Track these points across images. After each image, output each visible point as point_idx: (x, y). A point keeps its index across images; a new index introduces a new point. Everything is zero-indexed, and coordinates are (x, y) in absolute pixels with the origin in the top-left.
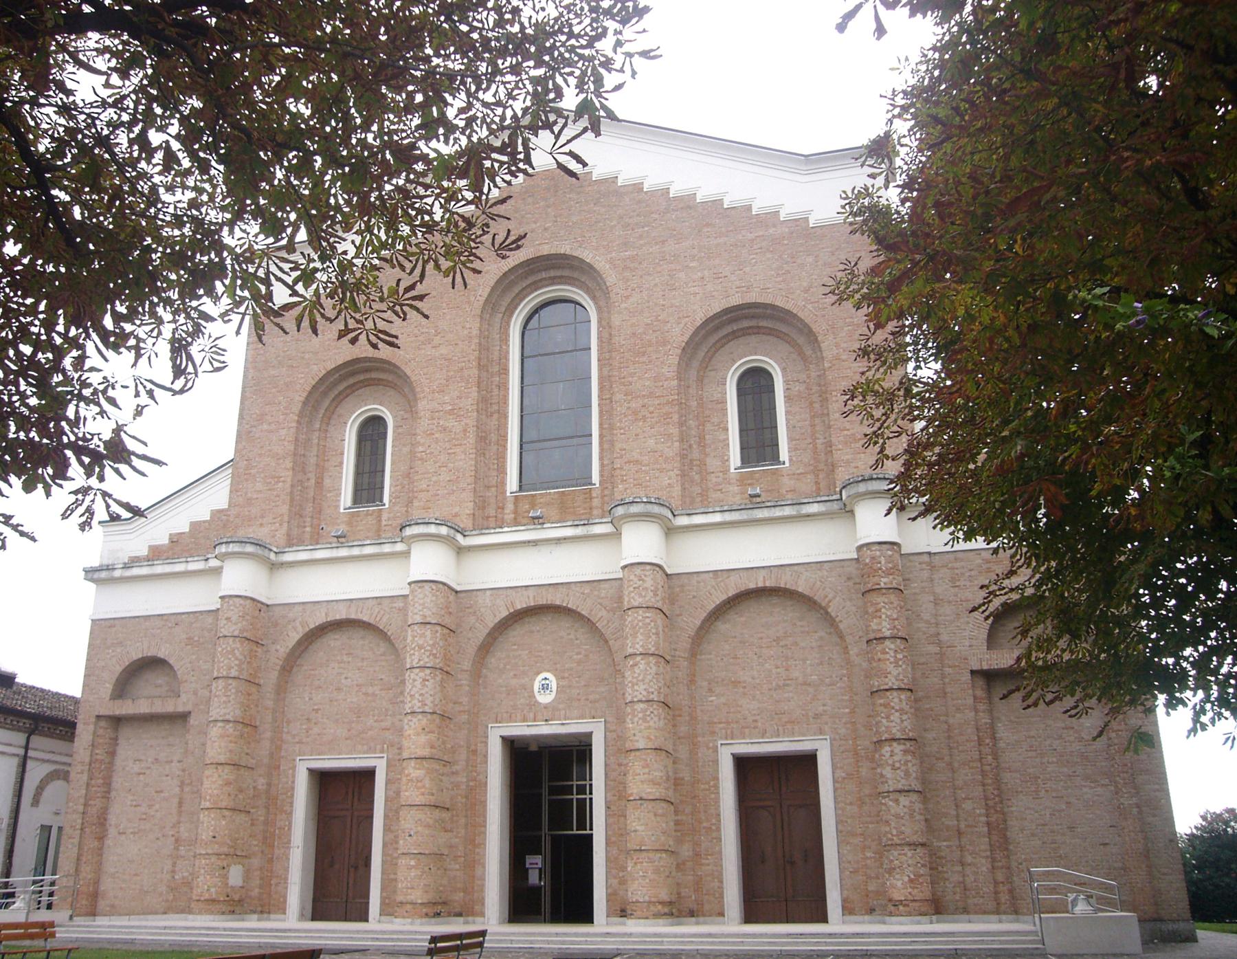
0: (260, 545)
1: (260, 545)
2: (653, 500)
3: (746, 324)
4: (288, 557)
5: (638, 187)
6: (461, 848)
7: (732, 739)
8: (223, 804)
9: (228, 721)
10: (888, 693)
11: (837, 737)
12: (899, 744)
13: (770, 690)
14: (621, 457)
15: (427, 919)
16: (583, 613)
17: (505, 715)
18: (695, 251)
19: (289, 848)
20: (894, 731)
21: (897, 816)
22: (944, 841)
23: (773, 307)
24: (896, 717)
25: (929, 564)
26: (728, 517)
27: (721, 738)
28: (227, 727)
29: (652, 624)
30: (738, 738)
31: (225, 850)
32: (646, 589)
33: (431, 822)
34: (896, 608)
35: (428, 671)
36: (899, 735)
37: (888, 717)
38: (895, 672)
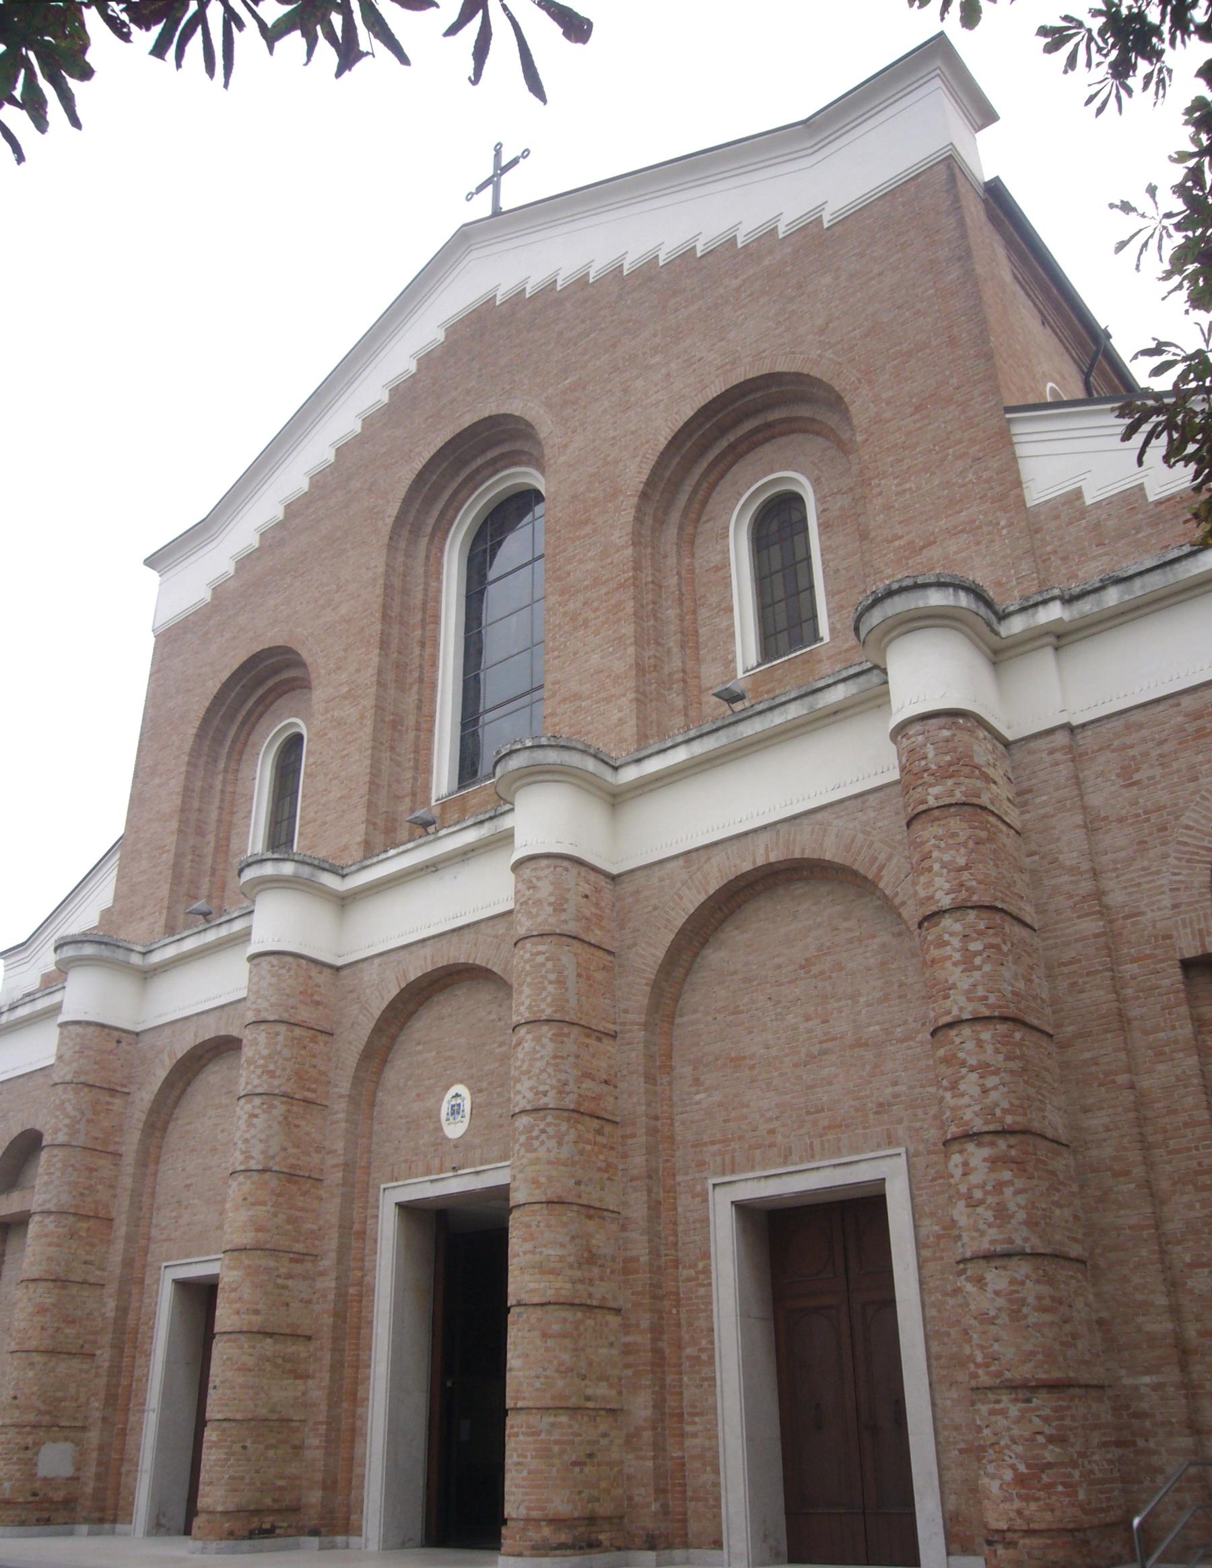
0: (106, 944)
1: (106, 944)
2: (544, 741)
3: (748, 426)
4: (156, 958)
5: (581, 282)
6: (324, 1407)
7: (733, 1172)
8: (34, 1343)
9: (49, 1213)
10: (953, 1033)
11: (921, 1147)
12: (980, 1145)
13: (796, 1065)
14: (554, 695)
15: (232, 1543)
16: (495, 969)
17: (404, 1166)
18: (658, 340)
19: (143, 1411)
20: (968, 1115)
21: (985, 1319)
22: (1147, 1372)
23: (773, 378)
24: (970, 1083)
25: (1070, 749)
26: (698, 748)
27: (715, 1174)
28: (47, 1221)
29: (550, 965)
30: (742, 1171)
31: (31, 1417)
32: (538, 902)
33: (250, 1362)
34: (965, 844)
35: (257, 1101)
36: (978, 1125)
37: (954, 1086)
38: (965, 984)
